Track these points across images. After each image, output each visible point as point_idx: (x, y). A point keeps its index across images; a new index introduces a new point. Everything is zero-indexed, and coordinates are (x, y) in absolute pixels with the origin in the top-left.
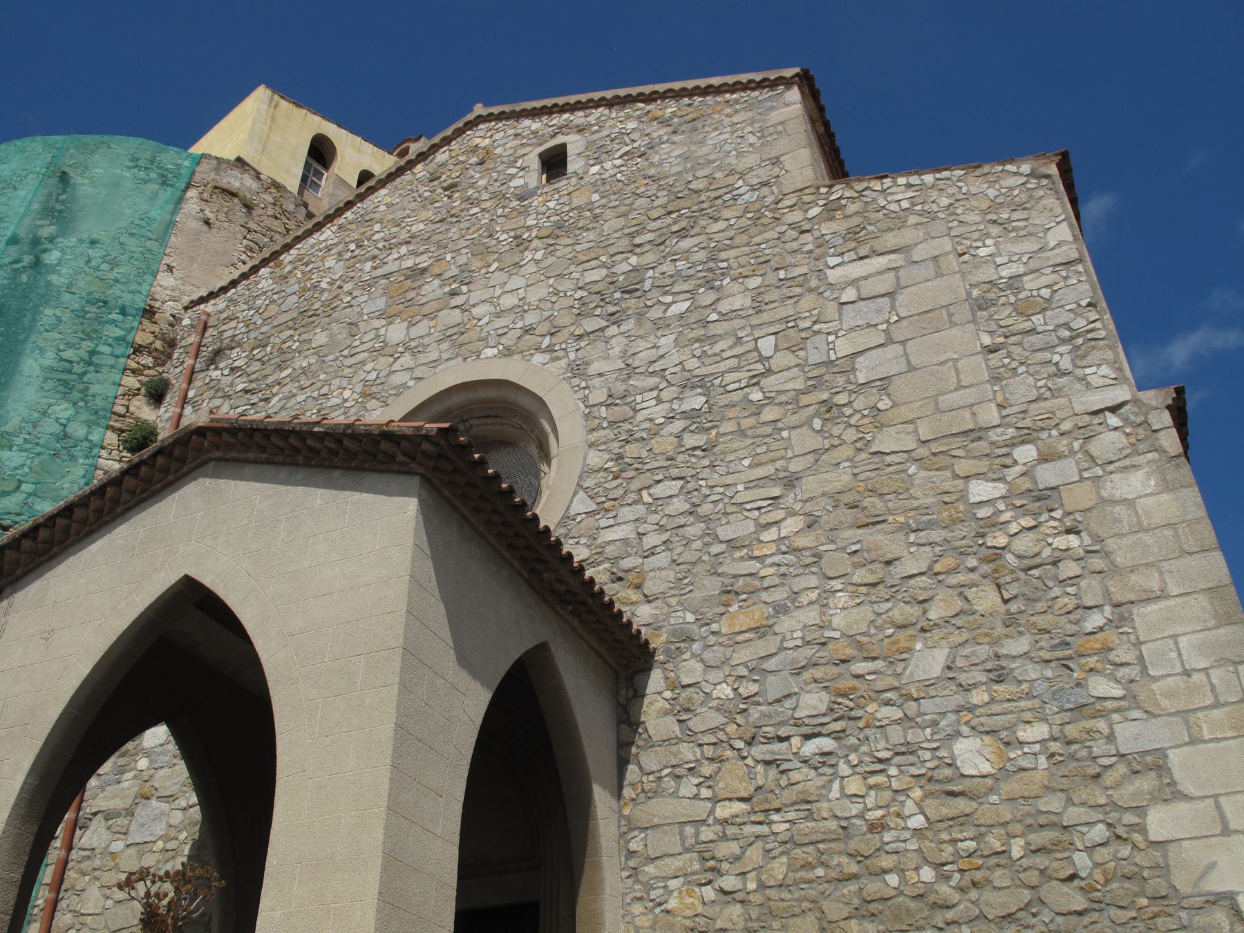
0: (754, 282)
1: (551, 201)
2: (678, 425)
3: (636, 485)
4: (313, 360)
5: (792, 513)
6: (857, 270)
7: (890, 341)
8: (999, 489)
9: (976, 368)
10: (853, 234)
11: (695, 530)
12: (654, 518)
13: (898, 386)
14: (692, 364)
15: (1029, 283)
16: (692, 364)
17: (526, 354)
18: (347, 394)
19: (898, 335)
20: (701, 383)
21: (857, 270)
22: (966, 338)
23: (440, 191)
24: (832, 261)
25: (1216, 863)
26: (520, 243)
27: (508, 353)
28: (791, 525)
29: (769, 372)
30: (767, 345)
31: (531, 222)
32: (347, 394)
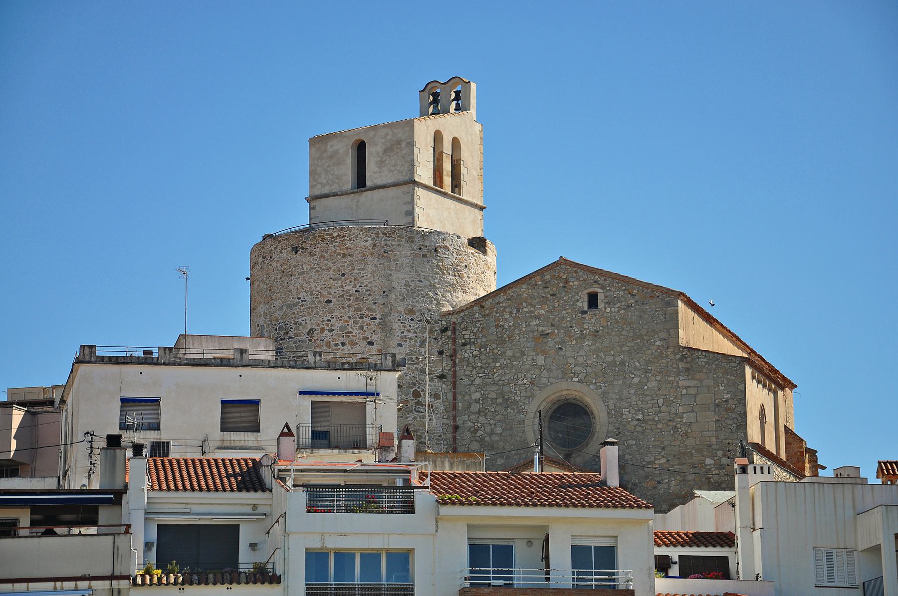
0: (658, 378)
1: (592, 321)
2: (635, 423)
3: (623, 439)
4: (509, 361)
5: (663, 457)
6: (687, 383)
7: (693, 411)
8: (713, 462)
9: (712, 426)
10: (687, 369)
11: (638, 457)
12: (627, 451)
13: (694, 426)
14: (639, 403)
15: (731, 402)
16: (639, 403)
17: (588, 383)
18: (525, 381)
19: (696, 410)
20: (640, 410)
21: (687, 383)
22: (711, 416)
23: (314, 327)
24: (681, 378)
25: (793, 386)
26: (582, 337)
27: (581, 381)
28: (663, 461)
29: (660, 412)
30: (660, 402)
31: (586, 327)
32: (525, 381)
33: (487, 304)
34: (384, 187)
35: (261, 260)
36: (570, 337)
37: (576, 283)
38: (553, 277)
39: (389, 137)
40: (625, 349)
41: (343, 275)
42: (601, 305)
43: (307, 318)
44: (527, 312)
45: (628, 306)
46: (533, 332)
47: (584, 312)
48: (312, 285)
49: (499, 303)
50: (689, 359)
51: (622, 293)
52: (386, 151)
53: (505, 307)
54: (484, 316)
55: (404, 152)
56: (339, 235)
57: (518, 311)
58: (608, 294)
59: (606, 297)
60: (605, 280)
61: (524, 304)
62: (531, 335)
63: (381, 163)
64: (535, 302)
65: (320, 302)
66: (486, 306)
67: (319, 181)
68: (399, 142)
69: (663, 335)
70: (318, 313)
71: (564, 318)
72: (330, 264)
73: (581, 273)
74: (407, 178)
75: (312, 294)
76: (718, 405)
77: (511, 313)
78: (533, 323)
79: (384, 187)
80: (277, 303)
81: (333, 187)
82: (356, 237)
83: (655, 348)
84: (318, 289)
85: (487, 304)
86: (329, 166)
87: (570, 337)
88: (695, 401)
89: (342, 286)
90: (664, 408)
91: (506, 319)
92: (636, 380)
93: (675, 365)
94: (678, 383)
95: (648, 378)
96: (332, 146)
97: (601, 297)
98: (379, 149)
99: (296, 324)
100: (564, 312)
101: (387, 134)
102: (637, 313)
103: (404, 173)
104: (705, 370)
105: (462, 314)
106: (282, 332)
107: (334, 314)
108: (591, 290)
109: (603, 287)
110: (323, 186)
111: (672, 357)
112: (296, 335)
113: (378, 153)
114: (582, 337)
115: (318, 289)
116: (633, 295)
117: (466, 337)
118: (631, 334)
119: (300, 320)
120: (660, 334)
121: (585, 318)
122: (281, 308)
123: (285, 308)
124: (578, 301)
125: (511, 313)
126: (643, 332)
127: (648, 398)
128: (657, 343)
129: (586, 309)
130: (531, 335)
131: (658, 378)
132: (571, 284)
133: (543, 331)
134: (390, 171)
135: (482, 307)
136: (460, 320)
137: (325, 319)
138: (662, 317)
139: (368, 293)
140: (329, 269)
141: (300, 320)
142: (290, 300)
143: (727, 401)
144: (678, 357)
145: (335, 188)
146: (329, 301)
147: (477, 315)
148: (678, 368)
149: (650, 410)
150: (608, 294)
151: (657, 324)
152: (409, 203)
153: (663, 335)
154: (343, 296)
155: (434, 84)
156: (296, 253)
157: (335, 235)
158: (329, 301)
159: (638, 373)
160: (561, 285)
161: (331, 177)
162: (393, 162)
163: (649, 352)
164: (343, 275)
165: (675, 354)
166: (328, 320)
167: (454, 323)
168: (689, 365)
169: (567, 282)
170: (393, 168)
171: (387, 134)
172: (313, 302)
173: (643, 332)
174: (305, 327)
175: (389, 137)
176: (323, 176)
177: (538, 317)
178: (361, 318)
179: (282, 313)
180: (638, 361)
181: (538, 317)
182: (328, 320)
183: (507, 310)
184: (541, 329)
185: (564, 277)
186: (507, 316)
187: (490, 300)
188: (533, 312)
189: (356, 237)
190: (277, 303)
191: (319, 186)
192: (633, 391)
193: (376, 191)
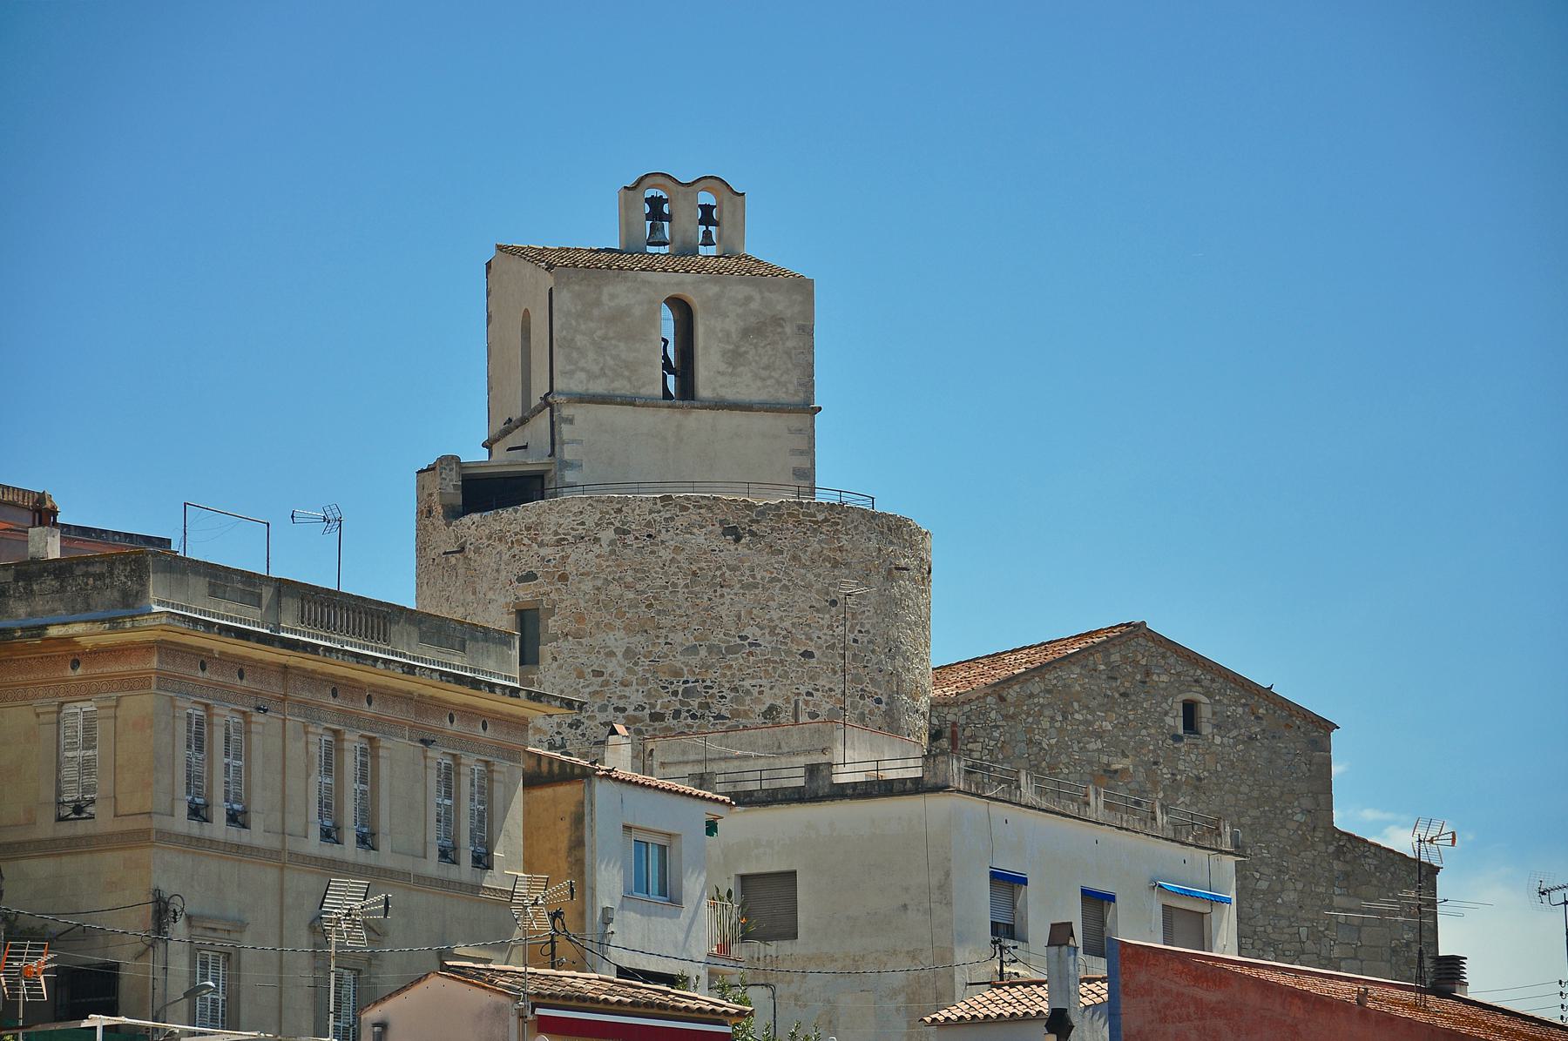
1: (1189, 760)
7: (1355, 958)
10: (1347, 875)
14: (1269, 929)
16: (1269, 929)
23: (779, 702)
24: (1337, 891)
26: (1175, 786)
31: (1181, 767)
33: (1012, 693)
34: (747, 407)
35: (608, 535)
36: (1155, 783)
37: (1164, 678)
38: (1125, 658)
39: (754, 306)
40: (1246, 820)
41: (834, 603)
42: (1206, 729)
43: (764, 682)
44: (1081, 722)
45: (1250, 738)
46: (1090, 763)
47: (1177, 738)
48: (775, 615)
49: (1031, 696)
50: (1349, 856)
51: (1240, 710)
52: (745, 333)
53: (1042, 706)
54: (1005, 717)
55: (790, 344)
56: (826, 520)
57: (1065, 718)
58: (1218, 708)
59: (1214, 714)
60: (1213, 680)
61: (1076, 705)
62: (1088, 769)
63: (735, 357)
64: (1093, 704)
65: (789, 652)
66: (1009, 699)
67: (582, 363)
68: (778, 321)
69: (1307, 803)
70: (786, 675)
71: (1143, 744)
72: (810, 576)
73: (1172, 661)
74: (797, 399)
75: (772, 632)
76: (1394, 951)
77: (1052, 719)
78: (1092, 746)
79: (747, 407)
80: (677, 637)
81: (616, 384)
82: (856, 527)
83: (1294, 826)
84: (787, 624)
85: (1012, 693)
86: (604, 338)
87: (1155, 783)
88: (1359, 939)
89: (830, 627)
90: (1309, 945)
91: (1044, 731)
92: (1263, 885)
93: (1324, 864)
94: (1332, 901)
95: (1282, 882)
96: (612, 297)
97: (1205, 712)
98: (732, 325)
99: (735, 689)
100: (1144, 732)
101: (749, 299)
102: (1265, 754)
103: (791, 388)
104: (1375, 882)
105: (967, 708)
106: (695, 703)
107: (821, 682)
108: (1188, 696)
109: (1209, 694)
110: (592, 376)
111: (1322, 847)
112: (736, 714)
113: (728, 335)
114: (1175, 786)
115: (787, 624)
116: (1258, 718)
117: (976, 755)
118: (1256, 794)
119: (747, 684)
120: (1303, 801)
121: (1178, 749)
122: (693, 650)
123: (703, 652)
124: (1166, 714)
125: (1052, 719)
126: (1275, 792)
127: (1284, 923)
128: (1298, 817)
129: (1181, 731)
130: (1088, 769)
131: (1300, 886)
132: (1155, 677)
133: (1108, 765)
134: (756, 376)
135: (1002, 699)
136: (963, 720)
137: (803, 690)
138: (1304, 768)
139: (871, 646)
140: (808, 586)
141: (747, 684)
142: (717, 638)
143: (1408, 945)
144: (1331, 849)
145: (621, 387)
146: (808, 655)
147: (993, 714)
148: (1331, 871)
149: (1287, 946)
150: (1218, 708)
151: (1297, 779)
152: (802, 453)
153: (1307, 803)
154: (833, 647)
155: (659, 180)
156: (737, 540)
157: (820, 517)
158: (808, 655)
159: (1266, 871)
160: (1138, 677)
161: (611, 362)
162: (765, 360)
163: (1283, 833)
164: (834, 603)
165: (1328, 844)
166: (809, 694)
167: (954, 724)
168: (1349, 868)
169: (1148, 674)
170: (764, 373)
171: (749, 299)
172: (776, 650)
173: (1275, 792)
174: (756, 701)
175: (754, 306)
176: (591, 355)
177: (1099, 735)
178: (862, 697)
179: (694, 660)
180: (1267, 847)
181: (1099, 735)
182: (809, 694)
183: (1047, 713)
184: (1105, 759)
185: (1143, 662)
186: (1045, 724)
187: (1017, 688)
188: (1090, 723)
189: (856, 527)
190: (677, 637)
191: (583, 376)
192: (1258, 905)
193: (723, 415)
